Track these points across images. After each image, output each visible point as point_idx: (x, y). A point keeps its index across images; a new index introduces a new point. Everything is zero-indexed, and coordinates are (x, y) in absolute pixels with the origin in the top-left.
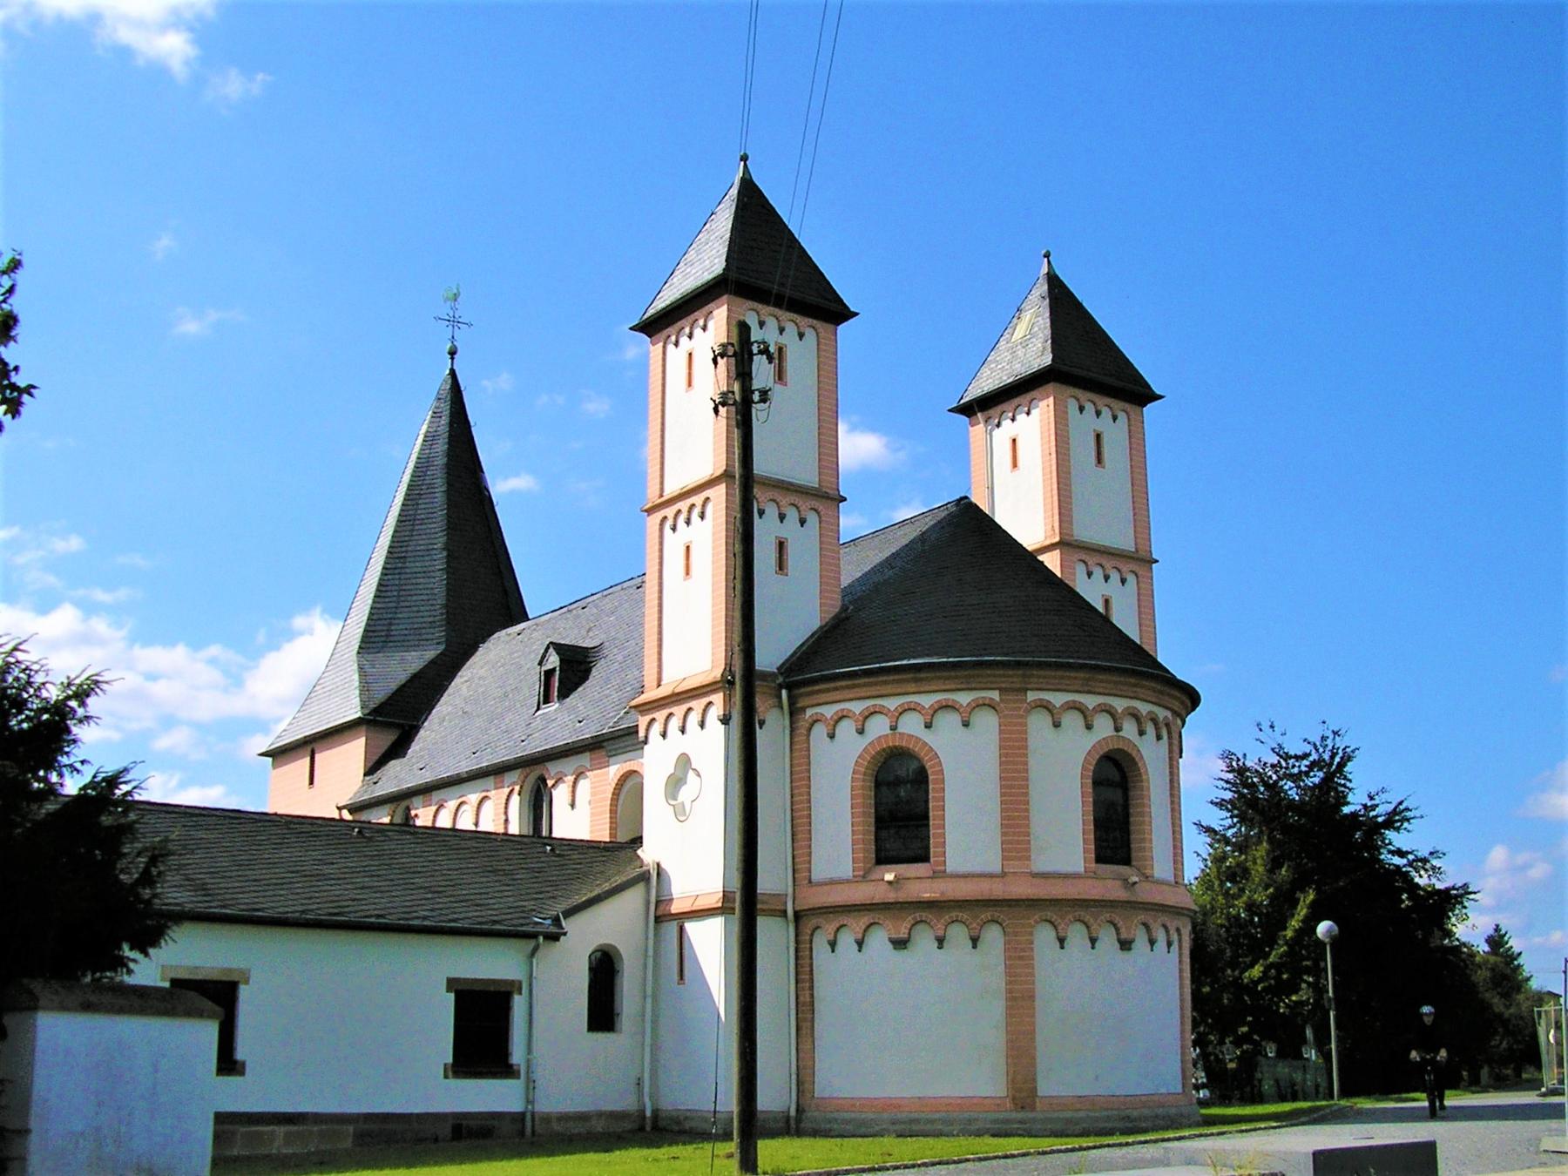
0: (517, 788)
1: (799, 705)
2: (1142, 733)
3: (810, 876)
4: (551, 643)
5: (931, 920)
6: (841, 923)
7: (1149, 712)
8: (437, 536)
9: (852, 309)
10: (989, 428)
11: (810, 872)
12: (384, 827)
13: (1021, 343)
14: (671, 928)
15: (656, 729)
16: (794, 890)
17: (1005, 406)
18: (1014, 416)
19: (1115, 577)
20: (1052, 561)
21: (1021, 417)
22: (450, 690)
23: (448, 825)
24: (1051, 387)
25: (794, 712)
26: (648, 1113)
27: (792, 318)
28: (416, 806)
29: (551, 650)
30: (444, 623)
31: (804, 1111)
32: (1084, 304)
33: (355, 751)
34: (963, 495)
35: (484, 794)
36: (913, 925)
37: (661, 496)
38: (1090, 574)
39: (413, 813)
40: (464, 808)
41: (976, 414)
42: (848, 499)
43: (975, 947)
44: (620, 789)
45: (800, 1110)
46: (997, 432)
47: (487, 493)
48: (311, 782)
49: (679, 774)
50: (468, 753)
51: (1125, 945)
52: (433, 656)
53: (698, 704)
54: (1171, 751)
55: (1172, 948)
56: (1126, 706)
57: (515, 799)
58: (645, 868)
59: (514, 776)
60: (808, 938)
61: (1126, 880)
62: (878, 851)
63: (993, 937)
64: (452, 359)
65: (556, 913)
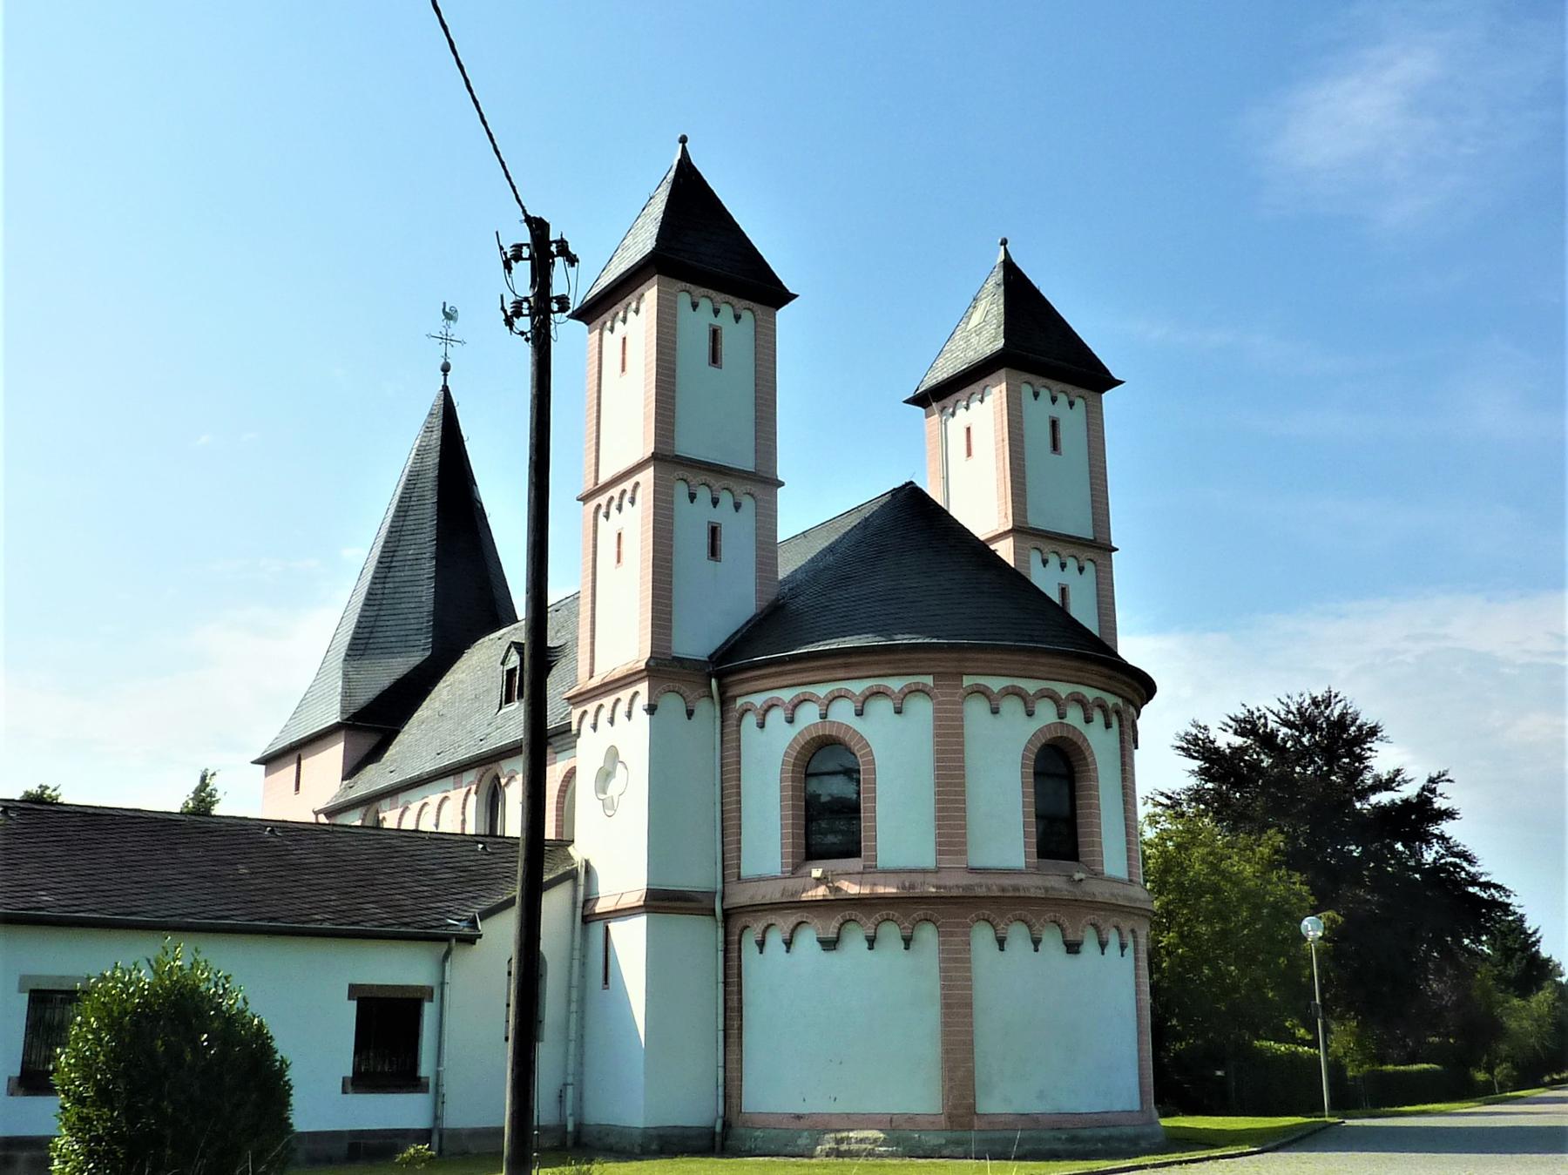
0: (474, 787)
1: (729, 694)
2: (1088, 720)
3: (739, 873)
4: (513, 642)
5: (861, 919)
6: (770, 922)
7: (1114, 704)
8: (425, 546)
9: (791, 291)
10: (944, 418)
11: (739, 868)
12: (390, 833)
13: (975, 331)
14: (597, 929)
15: (589, 720)
16: (724, 887)
17: (958, 395)
18: (968, 405)
19: (1072, 564)
20: (1005, 550)
21: (975, 405)
22: (433, 695)
23: (412, 827)
24: (1002, 373)
25: (725, 702)
26: (570, 1128)
27: (727, 300)
28: (384, 809)
29: (513, 649)
30: (431, 629)
31: (730, 1126)
32: (1041, 291)
33: (332, 757)
34: (908, 481)
35: (444, 795)
36: (842, 925)
37: (596, 484)
38: (1045, 562)
39: (381, 816)
40: (426, 809)
41: (931, 405)
42: (786, 483)
43: (907, 948)
44: (567, 786)
45: (727, 1125)
46: (951, 421)
47: (479, 505)
48: (297, 788)
49: (609, 768)
50: (434, 754)
51: (1073, 948)
52: (418, 662)
53: (625, 695)
54: (1122, 741)
55: (1126, 951)
56: (1069, 692)
57: (473, 798)
58: (575, 866)
59: (471, 776)
60: (736, 938)
61: (1071, 876)
62: (808, 846)
63: (928, 936)
64: (445, 375)
65: (472, 914)
